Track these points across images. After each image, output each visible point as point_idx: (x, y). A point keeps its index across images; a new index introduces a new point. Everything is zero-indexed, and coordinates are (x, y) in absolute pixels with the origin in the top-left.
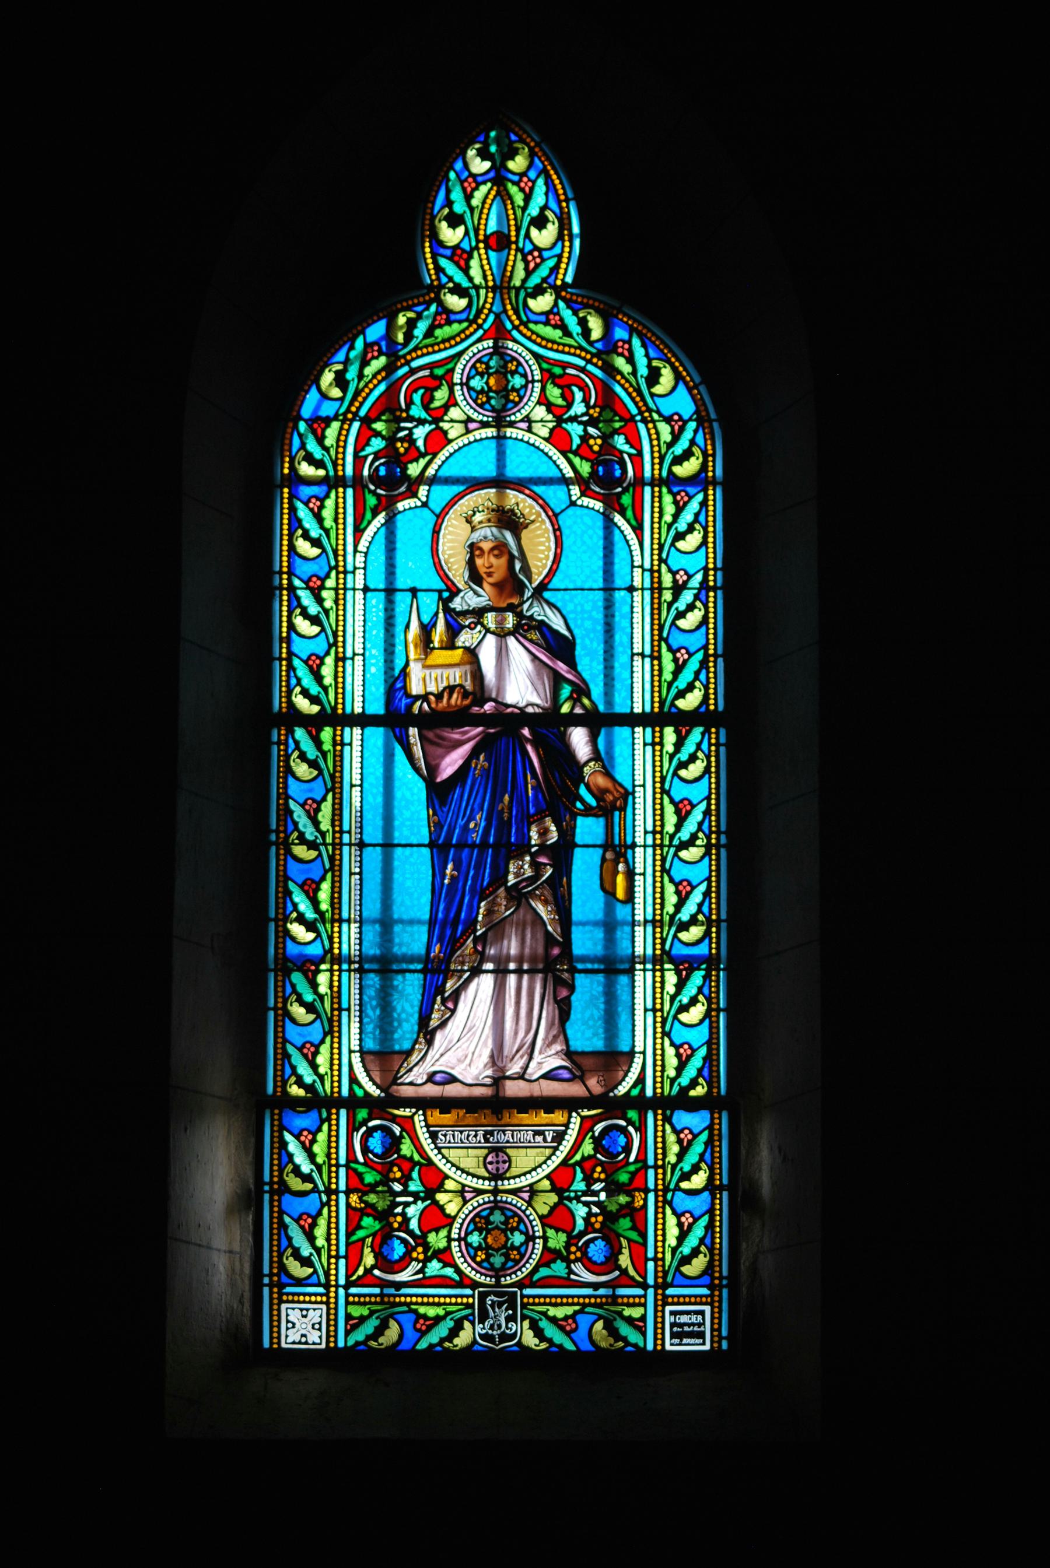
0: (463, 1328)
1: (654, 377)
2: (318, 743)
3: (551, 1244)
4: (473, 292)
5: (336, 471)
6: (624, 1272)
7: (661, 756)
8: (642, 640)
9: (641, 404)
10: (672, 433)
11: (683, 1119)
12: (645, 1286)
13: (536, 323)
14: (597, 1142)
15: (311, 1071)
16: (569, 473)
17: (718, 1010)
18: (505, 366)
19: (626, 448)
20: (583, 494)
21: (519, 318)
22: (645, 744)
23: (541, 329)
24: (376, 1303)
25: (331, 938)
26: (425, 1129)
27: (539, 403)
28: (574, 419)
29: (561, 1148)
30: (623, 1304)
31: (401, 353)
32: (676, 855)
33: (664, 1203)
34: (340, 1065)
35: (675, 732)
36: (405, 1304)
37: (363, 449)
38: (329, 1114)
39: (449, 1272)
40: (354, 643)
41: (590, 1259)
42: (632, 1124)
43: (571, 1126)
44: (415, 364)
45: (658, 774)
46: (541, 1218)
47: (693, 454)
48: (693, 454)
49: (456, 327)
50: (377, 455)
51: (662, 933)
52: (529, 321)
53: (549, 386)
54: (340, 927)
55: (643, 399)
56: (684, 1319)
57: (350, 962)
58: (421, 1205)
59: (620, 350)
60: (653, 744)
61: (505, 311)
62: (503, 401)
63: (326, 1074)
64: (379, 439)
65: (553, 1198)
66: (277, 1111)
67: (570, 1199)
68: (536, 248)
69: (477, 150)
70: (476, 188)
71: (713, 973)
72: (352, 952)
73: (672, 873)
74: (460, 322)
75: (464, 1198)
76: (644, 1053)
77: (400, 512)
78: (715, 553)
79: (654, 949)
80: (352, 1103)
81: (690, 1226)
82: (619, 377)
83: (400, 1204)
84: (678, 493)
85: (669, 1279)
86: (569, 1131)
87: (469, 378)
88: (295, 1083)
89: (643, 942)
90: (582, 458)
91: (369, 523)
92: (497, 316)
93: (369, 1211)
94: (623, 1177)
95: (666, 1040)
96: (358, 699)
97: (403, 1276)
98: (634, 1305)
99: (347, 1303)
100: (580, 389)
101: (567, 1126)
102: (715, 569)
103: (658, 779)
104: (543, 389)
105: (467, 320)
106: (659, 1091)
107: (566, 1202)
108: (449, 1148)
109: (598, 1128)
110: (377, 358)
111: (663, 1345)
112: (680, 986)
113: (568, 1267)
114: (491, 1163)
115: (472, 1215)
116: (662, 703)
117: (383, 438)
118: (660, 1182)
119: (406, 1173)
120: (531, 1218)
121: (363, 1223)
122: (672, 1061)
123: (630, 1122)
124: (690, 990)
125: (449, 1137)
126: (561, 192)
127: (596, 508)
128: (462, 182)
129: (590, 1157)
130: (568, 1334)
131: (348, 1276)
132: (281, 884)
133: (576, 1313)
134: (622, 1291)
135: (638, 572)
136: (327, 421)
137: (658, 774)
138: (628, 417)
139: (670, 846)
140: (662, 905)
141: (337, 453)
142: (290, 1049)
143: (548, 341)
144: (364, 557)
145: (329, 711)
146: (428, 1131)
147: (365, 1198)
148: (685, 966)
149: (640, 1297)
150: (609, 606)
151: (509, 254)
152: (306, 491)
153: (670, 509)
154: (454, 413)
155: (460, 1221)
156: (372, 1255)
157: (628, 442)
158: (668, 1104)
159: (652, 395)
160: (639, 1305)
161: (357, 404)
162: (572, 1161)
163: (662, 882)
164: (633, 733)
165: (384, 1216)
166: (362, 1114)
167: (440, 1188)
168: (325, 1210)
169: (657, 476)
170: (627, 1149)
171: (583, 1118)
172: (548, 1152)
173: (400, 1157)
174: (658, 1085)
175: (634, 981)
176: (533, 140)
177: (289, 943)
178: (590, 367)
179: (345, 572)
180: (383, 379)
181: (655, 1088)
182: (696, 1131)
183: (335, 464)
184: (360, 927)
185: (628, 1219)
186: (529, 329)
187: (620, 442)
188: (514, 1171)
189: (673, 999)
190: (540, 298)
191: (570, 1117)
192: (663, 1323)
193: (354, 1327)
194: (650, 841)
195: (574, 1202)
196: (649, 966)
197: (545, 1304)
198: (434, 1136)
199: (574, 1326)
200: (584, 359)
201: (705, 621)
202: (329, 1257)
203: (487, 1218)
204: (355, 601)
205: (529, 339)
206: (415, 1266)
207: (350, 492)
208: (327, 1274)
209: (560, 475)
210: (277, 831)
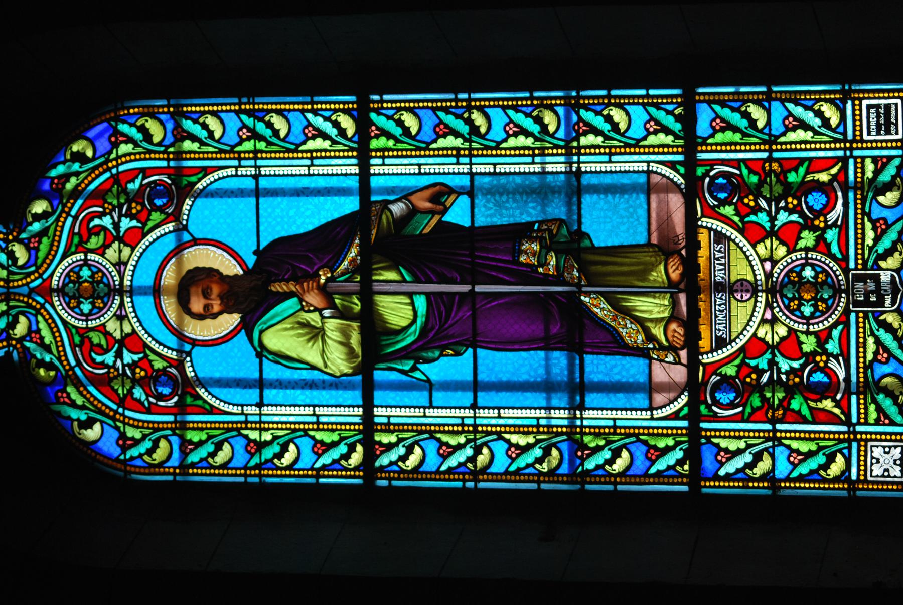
1: (80, 157)
2: (390, 447)
4: (13, 312)
5: (562, 434)
6: (834, 177)
7: (271, 152)
9: (101, 169)
10: (126, 142)
11: (703, 127)
12: (844, 160)
13: (37, 258)
14: (723, 203)
19: (138, 182)
21: (33, 273)
23: (41, 255)
24: (865, 399)
25: (488, 434)
26: (715, 354)
28: (116, 226)
30: (862, 178)
31: (63, 372)
33: (771, 141)
35: (585, 135)
36: (865, 373)
39: (836, 333)
41: (825, 206)
42: (708, 172)
43: (709, 225)
44: (73, 362)
46: (789, 252)
47: (143, 125)
48: (143, 125)
49: (42, 325)
52: (35, 264)
56: (873, 127)
57: (575, 418)
58: (779, 359)
61: (27, 284)
62: (825, 287)
63: (817, 444)
64: (134, 390)
67: (773, 226)
71: (582, 102)
72: (566, 416)
73: (499, 139)
74: (37, 322)
76: (648, 162)
77: (196, 375)
78: (222, 105)
80: (694, 417)
85: (841, 137)
86: (714, 227)
87: (82, 314)
89: (556, 165)
91: (205, 401)
93: (785, 404)
96: (350, 411)
97: (842, 375)
98: (863, 168)
99: (866, 423)
100: (93, 220)
101: (710, 230)
102: (240, 104)
107: (776, 229)
108: (730, 332)
111: (897, 141)
112: (194, 138)
113: (830, 227)
114: (742, 297)
115: (787, 313)
116: (352, 149)
117: (133, 387)
120: (789, 261)
123: (706, 174)
130: (889, 226)
131: (841, 423)
132: (442, 477)
133: (870, 220)
136: (123, 436)
138: (112, 180)
139: (470, 141)
140: (806, 142)
141: (148, 428)
142: (513, 468)
143: (51, 249)
145: (360, 437)
149: (856, 163)
155: (792, 323)
157: (133, 181)
158: (691, 142)
159: (94, 158)
160: (863, 163)
161: (107, 411)
164: (375, 174)
165: (790, 391)
166: (703, 409)
168: (715, 441)
171: (703, 216)
173: (737, 376)
177: (560, 471)
178: (73, 213)
179: (246, 422)
180: (86, 389)
182: (713, 116)
185: (788, 175)
187: (133, 186)
188: (750, 277)
189: (202, 143)
191: (702, 227)
192: (877, 141)
193: (887, 416)
194: (466, 160)
195: (776, 223)
196: (575, 158)
197: (863, 249)
200: (66, 219)
201: (214, 114)
203: (101, 282)
205: (49, 265)
206: (833, 364)
208: (840, 441)
210: (464, 481)
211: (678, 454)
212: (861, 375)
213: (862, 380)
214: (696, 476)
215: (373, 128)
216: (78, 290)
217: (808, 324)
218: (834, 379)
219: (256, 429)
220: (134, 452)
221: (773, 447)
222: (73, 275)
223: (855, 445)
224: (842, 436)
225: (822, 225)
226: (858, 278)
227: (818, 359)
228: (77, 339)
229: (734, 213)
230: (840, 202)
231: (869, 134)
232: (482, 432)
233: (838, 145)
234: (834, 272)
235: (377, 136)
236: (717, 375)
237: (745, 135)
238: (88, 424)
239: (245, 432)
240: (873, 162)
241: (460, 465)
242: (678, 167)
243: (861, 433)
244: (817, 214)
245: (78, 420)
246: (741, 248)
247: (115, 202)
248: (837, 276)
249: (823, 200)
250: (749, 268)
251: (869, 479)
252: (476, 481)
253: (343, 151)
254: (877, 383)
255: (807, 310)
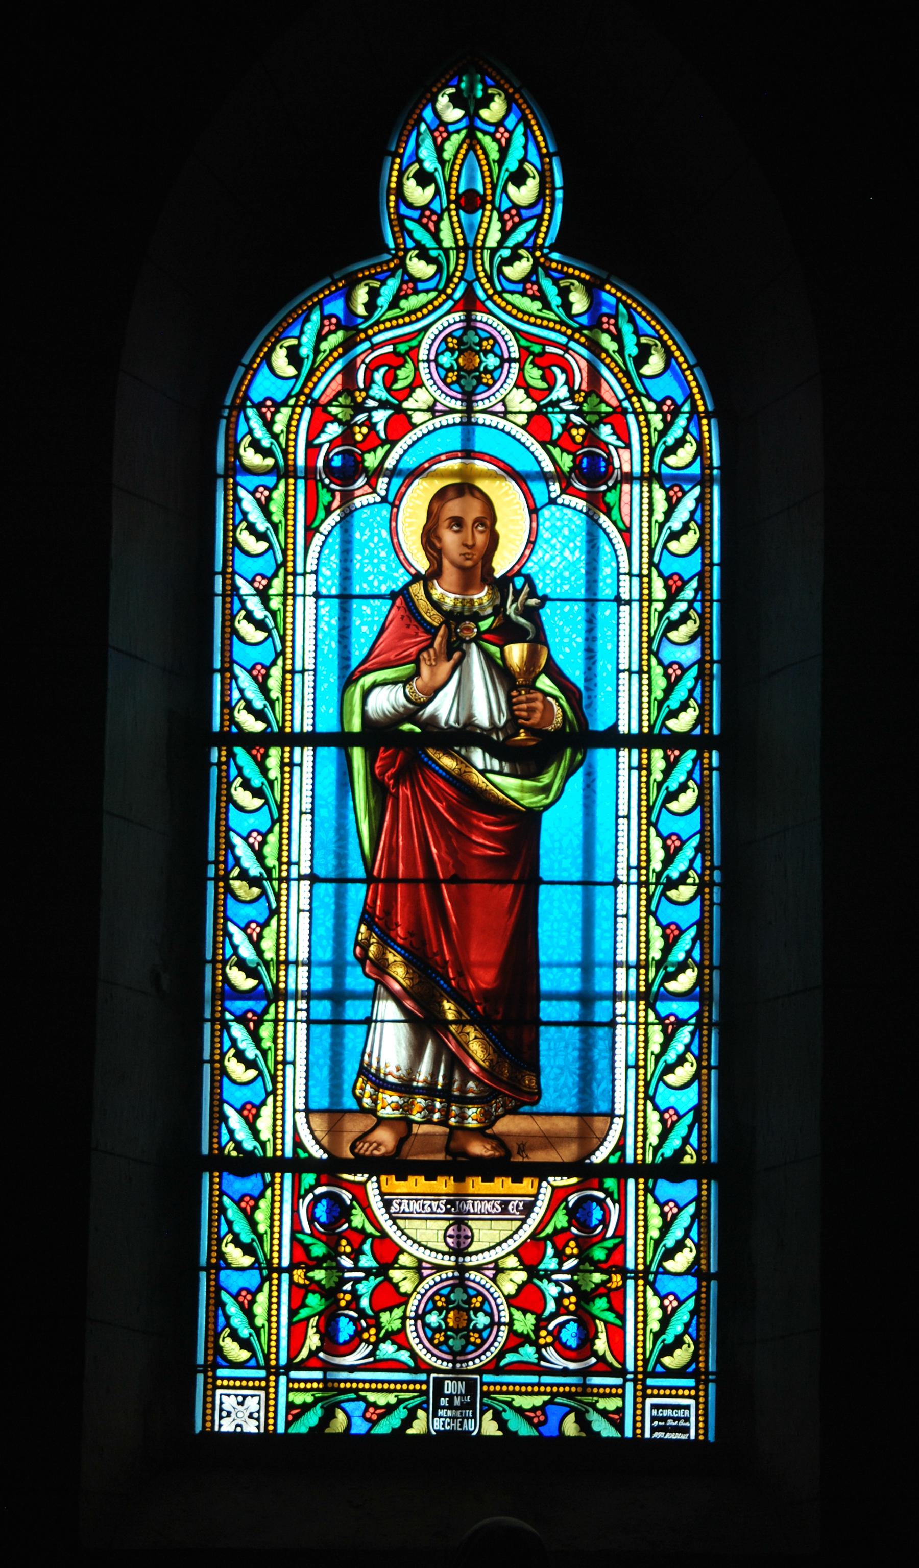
0: (416, 1418)
3: (519, 1327)
6: (602, 1359)
7: (644, 1335)
8: (629, 656)
11: (665, 1189)
12: (622, 1373)
13: (512, 292)
14: (570, 1212)
15: (248, 1228)
16: (549, 467)
17: (709, 1068)
18: (468, 1301)
19: (612, 439)
20: (563, 491)
22: (630, 768)
23: (516, 299)
25: (278, 896)
26: (379, 1198)
27: (517, 386)
29: (529, 1221)
31: (363, 326)
32: (663, 894)
34: (283, 1132)
36: (350, 1390)
37: (318, 436)
38: (273, 1177)
39: (404, 1356)
40: (304, 656)
41: (564, 1345)
43: (541, 1197)
44: (377, 339)
45: (645, 633)
46: (508, 1298)
49: (423, 298)
50: (333, 443)
51: (647, 974)
52: (504, 290)
53: (528, 366)
54: (286, 970)
55: (630, 381)
56: (668, 1413)
58: (373, 1281)
59: (605, 326)
60: (640, 768)
61: (478, 279)
63: (263, 1326)
64: (336, 424)
65: (522, 1276)
66: (216, 1174)
68: (515, 206)
69: (450, 95)
70: (448, 139)
73: (662, 567)
74: (427, 291)
75: (421, 1275)
76: (625, 1116)
77: (357, 509)
79: (642, 467)
81: (675, 1310)
82: (604, 355)
83: (349, 1280)
84: (671, 488)
85: (650, 1368)
86: (539, 1203)
88: (232, 1242)
90: (563, 450)
92: (470, 285)
94: (599, 1254)
95: (652, 829)
98: (610, 1396)
99: (289, 1390)
100: (563, 371)
101: (536, 1196)
103: (645, 639)
104: (522, 370)
105: (435, 289)
106: (640, 1157)
109: (573, 1199)
110: (334, 332)
113: (538, 1351)
114: (451, 1236)
116: (651, 727)
117: (340, 422)
118: (640, 1261)
119: (356, 1247)
121: (308, 1301)
122: (655, 1128)
123: (609, 1194)
124: (679, 776)
125: (404, 1206)
126: (542, 144)
127: (579, 508)
128: (432, 132)
129: (563, 1230)
131: (290, 1358)
133: (545, 1403)
134: (596, 1380)
135: (625, 580)
136: (278, 406)
137: (645, 633)
139: (657, 884)
140: (645, 1136)
141: (288, 440)
142: (225, 1297)
144: (319, 562)
145: (276, 729)
146: (383, 1200)
147: (310, 1274)
148: (674, 485)
149: (617, 1387)
150: (591, 622)
151: (483, 215)
152: (240, 1006)
153: (661, 505)
154: (419, 393)
156: (317, 1336)
160: (616, 1395)
161: (311, 385)
162: (543, 1235)
163: (645, 1111)
166: (308, 1179)
167: (392, 1264)
168: (268, 1192)
169: (645, 484)
170: (605, 1221)
171: (554, 1188)
172: (518, 1223)
174: (640, 1151)
175: (614, 1036)
176: (512, 86)
179: (294, 574)
180: (340, 356)
181: (636, 1155)
183: (285, 453)
184: (309, 971)
186: (504, 299)
187: (605, 432)
190: (517, 264)
191: (540, 1187)
193: (297, 1418)
194: (634, 878)
195: (545, 1281)
198: (387, 1204)
199: (542, 1418)
202: (276, 1063)
203: (447, 1296)
204: (305, 609)
205: (503, 310)
206: (364, 1350)
207: (301, 484)
208: (267, 1357)
209: (538, 469)
211: (249, 1144)
212: (348, 1385)
213: (342, 1385)
214: (222, 1163)
215: (677, 752)
216: (471, 349)
217: (416, 1318)
218: (343, 1349)
219: (286, 587)
220: (256, 423)
221: (260, 1269)
222: (493, 345)
223: (262, 1373)
224: (273, 1356)
225: (542, 1341)
226: (471, 1387)
227: (373, 1331)
228: (403, 348)
229: (559, 1227)
230: (572, 1366)
231: (654, 1406)
232: (280, 889)
233: (640, 1363)
234: (479, 1357)
235: (666, 757)
236: (351, 1201)
237: (660, 785)
238: (294, 357)
239: (281, 573)
240: (618, 1408)
241: (237, 860)
242: (618, 1154)
243: (277, 1381)
244: (556, 1334)
245: (299, 345)
246: (511, 1236)
247: (585, 408)
248: (473, 1359)
249: (573, 1343)
250: (486, 1246)
251: (219, 1392)
252: (217, 879)
253: (645, 1258)
254: (338, 1405)
255: (433, 1319)
